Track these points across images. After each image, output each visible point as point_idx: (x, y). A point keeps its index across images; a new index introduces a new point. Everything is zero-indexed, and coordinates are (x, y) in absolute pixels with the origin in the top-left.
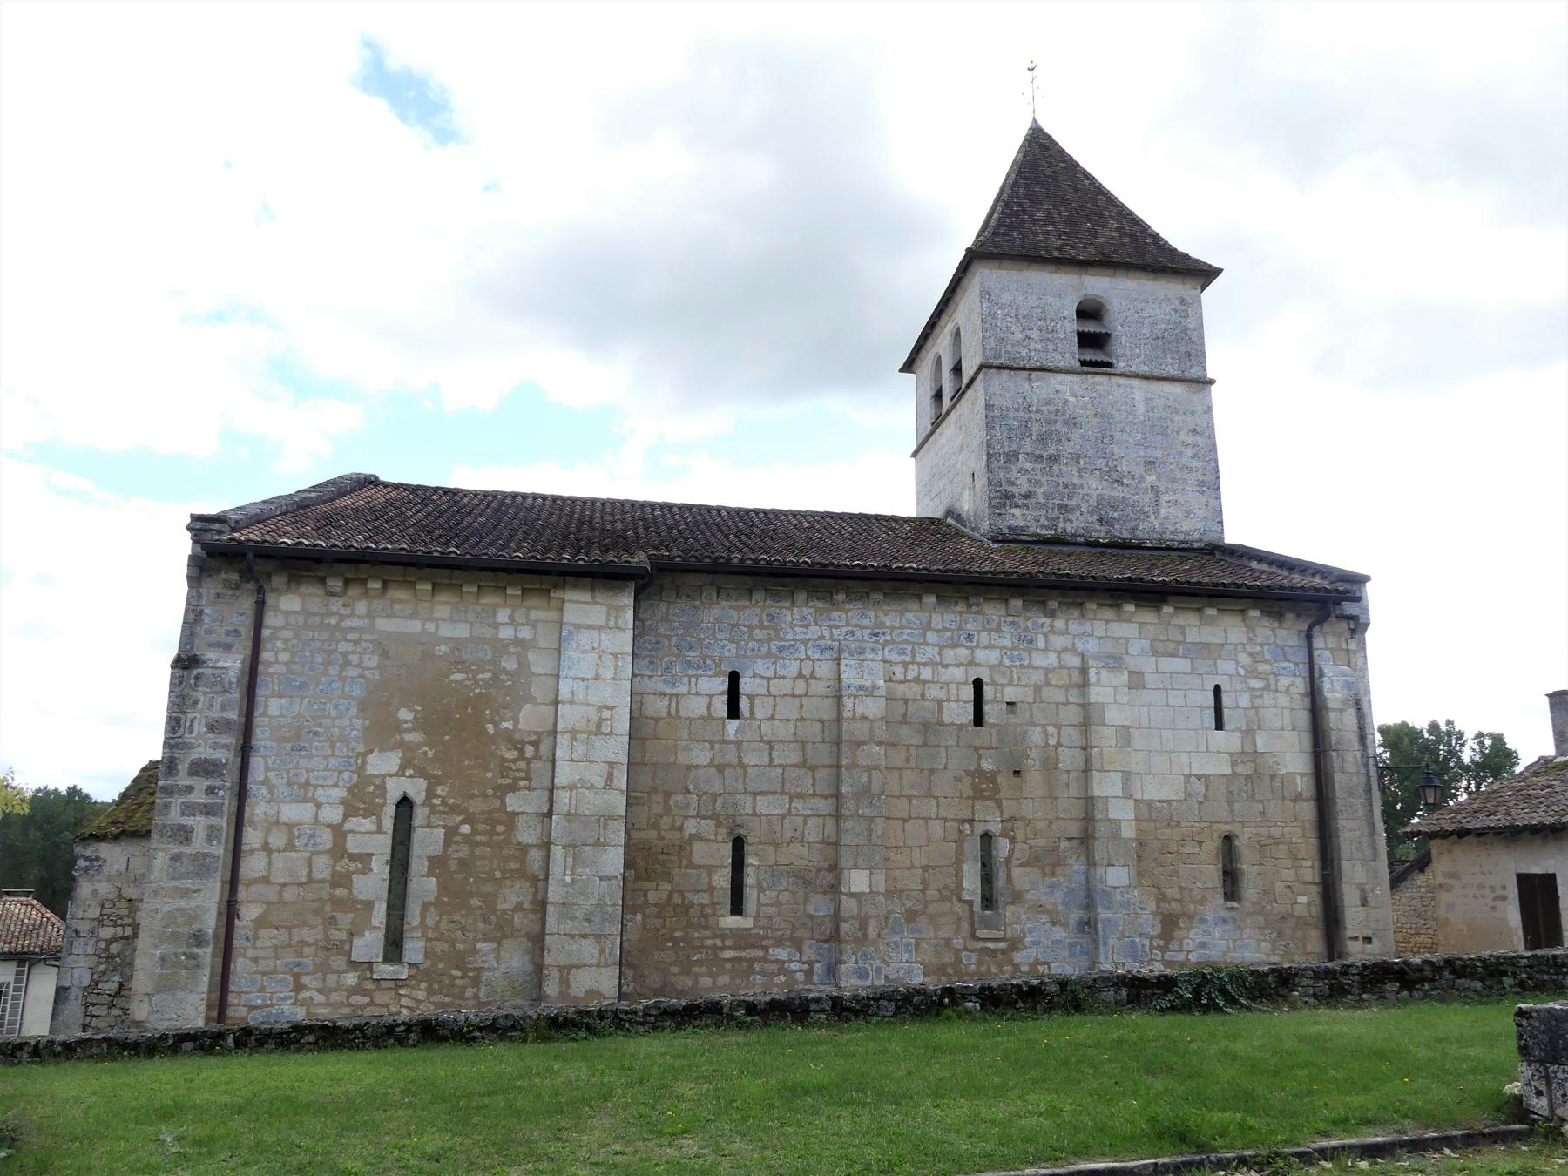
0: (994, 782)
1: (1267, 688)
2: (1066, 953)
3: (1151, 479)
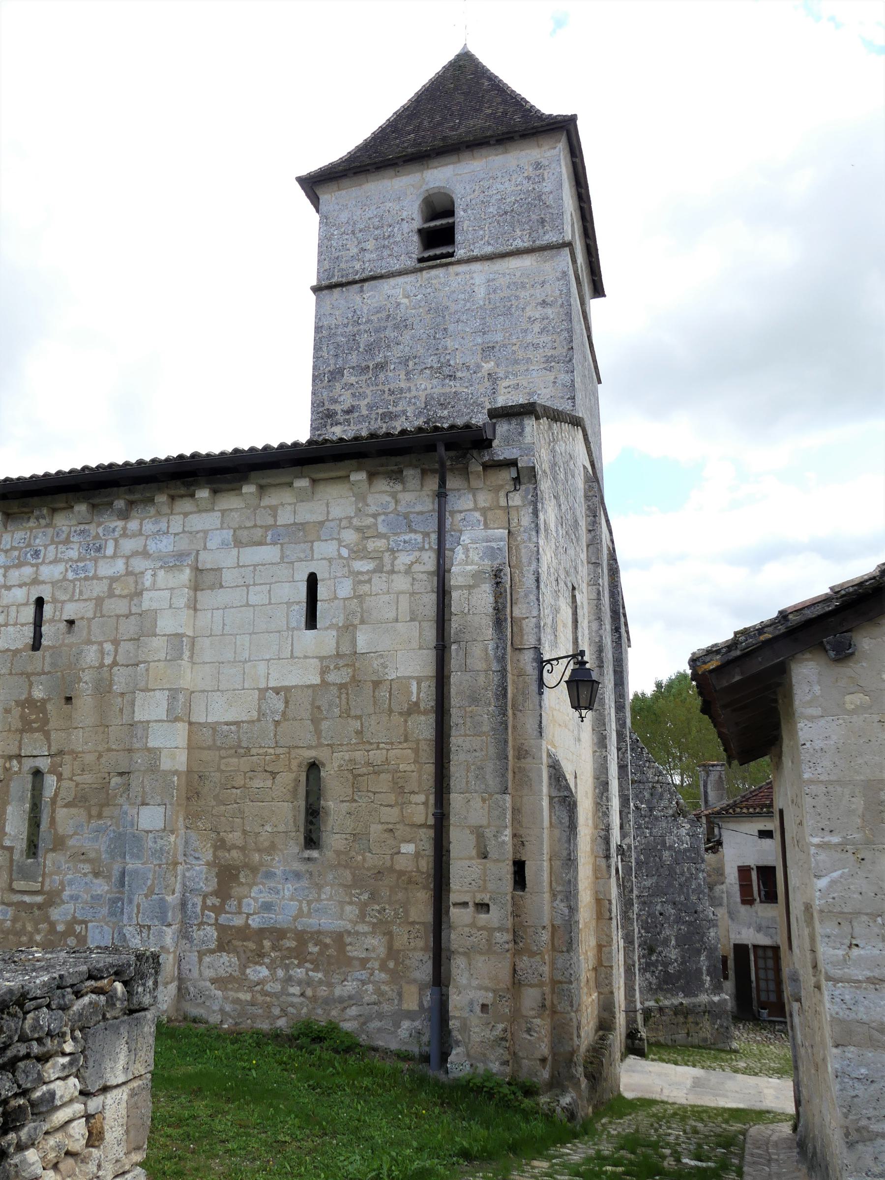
0: (44, 711)
1: (379, 570)
2: (105, 910)
3: (488, 366)
